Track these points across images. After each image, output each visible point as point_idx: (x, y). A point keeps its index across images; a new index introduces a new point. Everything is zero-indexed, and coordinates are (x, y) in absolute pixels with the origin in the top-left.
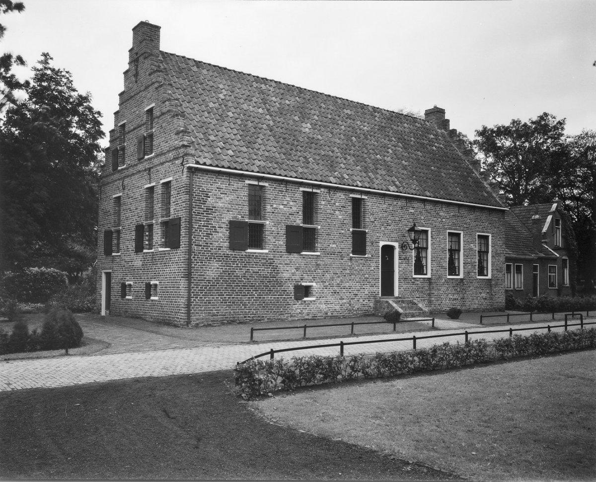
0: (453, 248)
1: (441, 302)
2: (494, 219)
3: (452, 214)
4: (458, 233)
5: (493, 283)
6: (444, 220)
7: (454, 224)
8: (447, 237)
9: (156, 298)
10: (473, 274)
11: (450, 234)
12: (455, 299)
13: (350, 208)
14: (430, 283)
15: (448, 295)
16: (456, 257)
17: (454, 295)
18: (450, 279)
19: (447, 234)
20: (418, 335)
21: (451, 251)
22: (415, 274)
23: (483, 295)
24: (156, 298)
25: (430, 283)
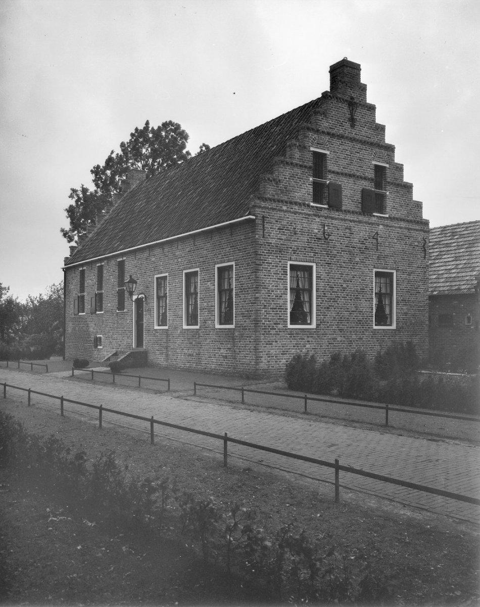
0: (383, 291)
1: (177, 357)
2: (238, 238)
3: (187, 250)
4: (194, 272)
5: (236, 334)
6: (180, 260)
7: (190, 261)
8: (374, 278)
9: (101, 347)
10: (210, 322)
11: (378, 274)
12: (190, 355)
13: (117, 271)
14: (168, 336)
15: (183, 349)
16: (387, 303)
17: (189, 350)
18: (292, 329)
19: (374, 273)
20: (309, 396)
21: (379, 295)
22: (376, 325)
23: (222, 351)
24: (101, 347)
25: (168, 336)
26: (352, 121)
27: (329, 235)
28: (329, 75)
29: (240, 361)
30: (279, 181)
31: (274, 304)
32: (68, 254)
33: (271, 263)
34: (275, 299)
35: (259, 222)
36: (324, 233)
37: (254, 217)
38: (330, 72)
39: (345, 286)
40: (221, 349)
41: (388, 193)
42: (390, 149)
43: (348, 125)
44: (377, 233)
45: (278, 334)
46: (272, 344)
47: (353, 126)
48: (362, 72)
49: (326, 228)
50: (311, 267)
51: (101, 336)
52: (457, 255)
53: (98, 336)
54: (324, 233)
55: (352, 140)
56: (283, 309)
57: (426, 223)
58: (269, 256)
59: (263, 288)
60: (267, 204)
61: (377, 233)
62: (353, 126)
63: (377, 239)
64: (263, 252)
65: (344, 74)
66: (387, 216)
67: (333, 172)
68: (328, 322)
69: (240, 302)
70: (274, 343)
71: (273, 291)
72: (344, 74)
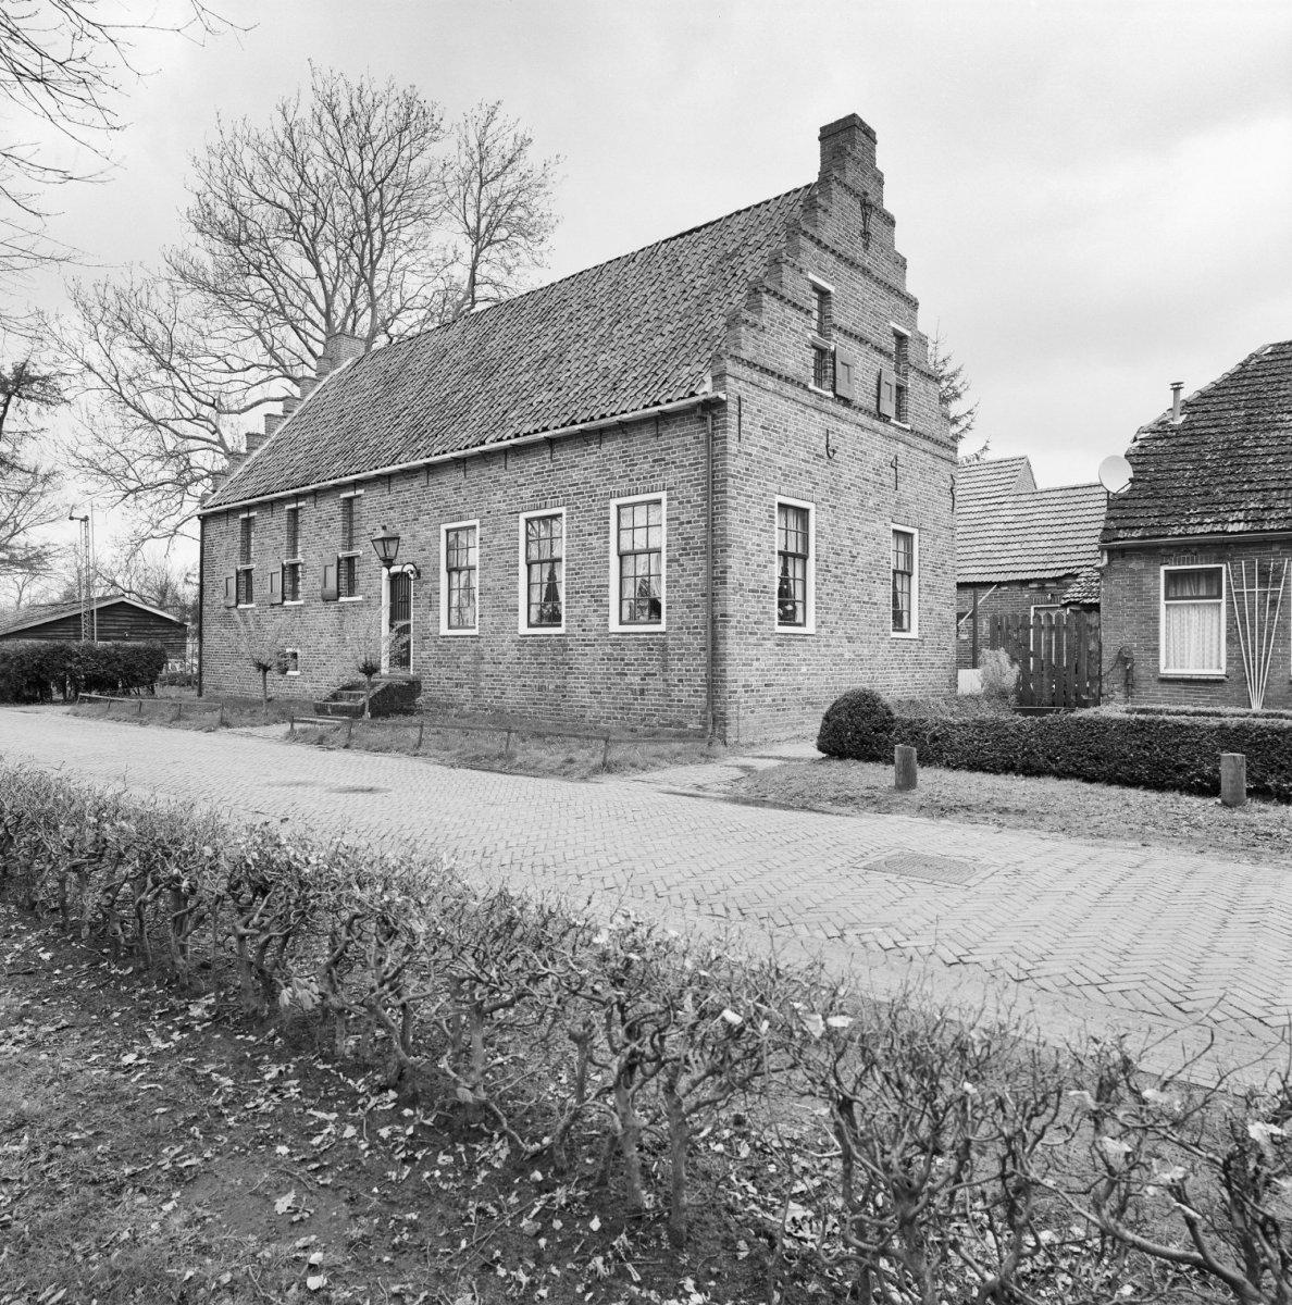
35: (732, 407)
38: (820, 139)
42: (913, 304)
55: (866, 272)
66: (908, 427)
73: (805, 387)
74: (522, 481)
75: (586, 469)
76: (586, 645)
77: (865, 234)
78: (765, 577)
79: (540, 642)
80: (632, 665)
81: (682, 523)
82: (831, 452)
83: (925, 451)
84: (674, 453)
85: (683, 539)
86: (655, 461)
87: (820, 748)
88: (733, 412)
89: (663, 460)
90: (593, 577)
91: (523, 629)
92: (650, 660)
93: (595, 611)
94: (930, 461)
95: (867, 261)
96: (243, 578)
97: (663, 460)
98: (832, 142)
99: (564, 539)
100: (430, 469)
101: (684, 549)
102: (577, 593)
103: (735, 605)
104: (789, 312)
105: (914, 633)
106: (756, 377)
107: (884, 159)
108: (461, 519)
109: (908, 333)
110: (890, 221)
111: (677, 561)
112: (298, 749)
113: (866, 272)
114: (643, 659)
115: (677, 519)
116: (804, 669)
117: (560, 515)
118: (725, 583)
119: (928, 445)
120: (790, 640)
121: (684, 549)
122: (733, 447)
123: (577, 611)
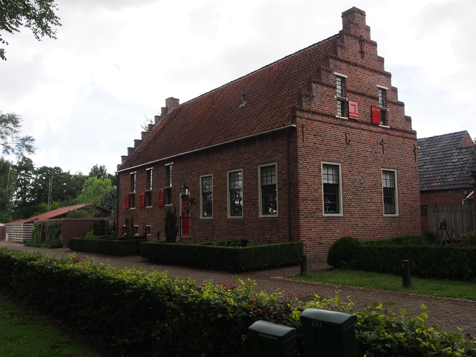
26: (362, 52)
27: (350, 141)
28: (341, 20)
29: (315, 240)
30: (313, 96)
31: (313, 196)
32: (120, 162)
33: (309, 163)
34: (313, 192)
35: (299, 129)
36: (346, 139)
37: (295, 126)
38: (342, 17)
39: (362, 181)
40: (265, 234)
41: (388, 110)
42: (388, 75)
43: (359, 56)
44: (382, 140)
45: (316, 222)
46: (312, 230)
47: (362, 57)
48: (367, 17)
49: (347, 136)
50: (338, 166)
51: (150, 226)
52: (425, 161)
53: (147, 226)
54: (346, 139)
55: (363, 67)
56: (319, 200)
57: (414, 133)
58: (307, 157)
59: (304, 183)
60: (306, 115)
61: (382, 140)
62: (362, 57)
63: (383, 145)
64: (303, 154)
65: (353, 18)
66: (389, 127)
67: (351, 92)
68: (352, 211)
69: (283, 195)
70: (313, 229)
71: (311, 186)
72: (353, 18)
73: (334, 117)
74: (227, 158)
75: (249, 154)
76: (251, 223)
77: (362, 52)
78: (317, 195)
79: (235, 221)
80: (267, 230)
81: (283, 174)
82: (348, 143)
83: (398, 136)
84: (279, 147)
85: (283, 180)
86: (273, 150)
87: (330, 264)
88: (300, 131)
89: (276, 150)
90: (253, 196)
91: (229, 216)
92: (273, 228)
93: (254, 209)
94: (400, 140)
95: (363, 63)
96: (131, 197)
97: (276, 150)
98: (345, 18)
99: (277, 176)
100: (238, 143)
101: (284, 184)
102: (247, 202)
103: (305, 207)
104: (325, 88)
105: (397, 215)
106: (310, 116)
107: (368, 22)
108: (207, 174)
109: (387, 88)
110: (374, 44)
111: (282, 189)
112: (26, 247)
113: (363, 67)
114: (271, 228)
115: (281, 173)
116: (338, 231)
117: (275, 165)
118: (298, 198)
119: (397, 133)
120: (331, 219)
121: (284, 184)
122: (300, 145)
123: (247, 209)
